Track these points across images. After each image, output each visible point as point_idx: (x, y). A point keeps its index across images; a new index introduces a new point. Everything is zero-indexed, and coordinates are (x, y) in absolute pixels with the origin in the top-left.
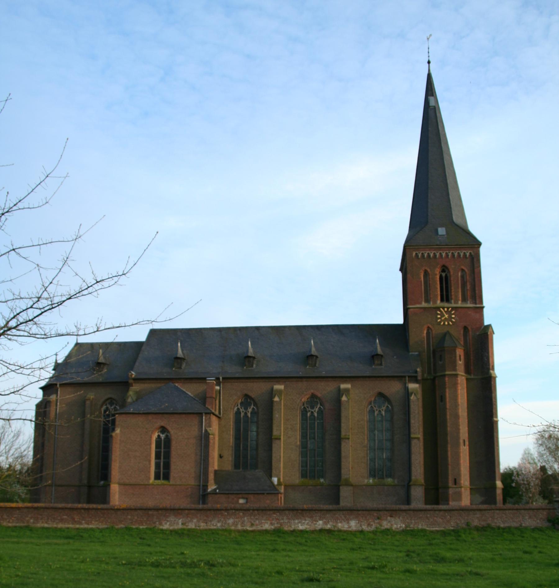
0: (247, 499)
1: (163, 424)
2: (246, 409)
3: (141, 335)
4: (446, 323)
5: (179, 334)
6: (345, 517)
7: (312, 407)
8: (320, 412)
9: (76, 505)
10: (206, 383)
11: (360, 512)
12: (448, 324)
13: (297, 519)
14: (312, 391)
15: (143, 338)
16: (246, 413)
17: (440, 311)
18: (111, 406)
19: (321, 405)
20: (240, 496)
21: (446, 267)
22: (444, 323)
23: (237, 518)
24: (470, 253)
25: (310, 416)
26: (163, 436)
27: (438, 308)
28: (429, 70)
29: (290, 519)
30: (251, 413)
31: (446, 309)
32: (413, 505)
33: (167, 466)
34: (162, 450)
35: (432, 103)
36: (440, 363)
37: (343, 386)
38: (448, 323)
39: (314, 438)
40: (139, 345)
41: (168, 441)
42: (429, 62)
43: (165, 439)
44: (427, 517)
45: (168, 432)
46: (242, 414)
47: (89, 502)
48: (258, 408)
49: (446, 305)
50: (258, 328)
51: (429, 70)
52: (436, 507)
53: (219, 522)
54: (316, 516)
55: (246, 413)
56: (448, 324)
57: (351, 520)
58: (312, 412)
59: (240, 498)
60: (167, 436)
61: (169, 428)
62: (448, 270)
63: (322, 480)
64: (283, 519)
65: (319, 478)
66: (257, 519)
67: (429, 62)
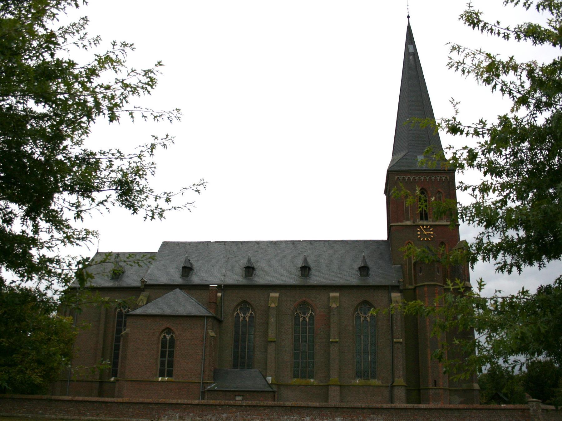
0: (243, 396)
1: (168, 326)
2: (244, 314)
3: (155, 248)
4: (425, 239)
5: (180, 245)
6: (331, 414)
7: (304, 314)
8: (311, 317)
9: (87, 398)
10: (209, 289)
11: (345, 410)
12: (427, 239)
13: (286, 415)
14: (304, 299)
15: (155, 249)
16: (244, 318)
17: (420, 228)
18: (125, 309)
19: (312, 311)
20: (237, 393)
21: (425, 190)
22: (418, 231)
23: (230, 413)
24: (446, 177)
25: (302, 321)
26: (168, 337)
27: (418, 226)
28: (409, 23)
29: (279, 415)
30: (249, 318)
31: (425, 227)
32: (398, 405)
33: (171, 364)
34: (167, 349)
35: (411, 50)
36: (420, 274)
37: (332, 294)
38: (427, 239)
39: (306, 342)
40: (151, 256)
41: (172, 342)
42: (408, 17)
43: (170, 339)
44: (408, 415)
45: (174, 333)
46: (241, 318)
47: (100, 395)
48: (255, 314)
49: (425, 223)
50: (257, 243)
51: (409, 23)
52: (416, 406)
53: (213, 416)
54: (304, 413)
55: (244, 318)
56: (427, 239)
57: (336, 417)
58: (304, 318)
59: (236, 395)
60: (172, 336)
61: (174, 329)
62: (427, 192)
63: (312, 380)
64: (272, 415)
65: (309, 378)
66: (248, 414)
67: (408, 17)
